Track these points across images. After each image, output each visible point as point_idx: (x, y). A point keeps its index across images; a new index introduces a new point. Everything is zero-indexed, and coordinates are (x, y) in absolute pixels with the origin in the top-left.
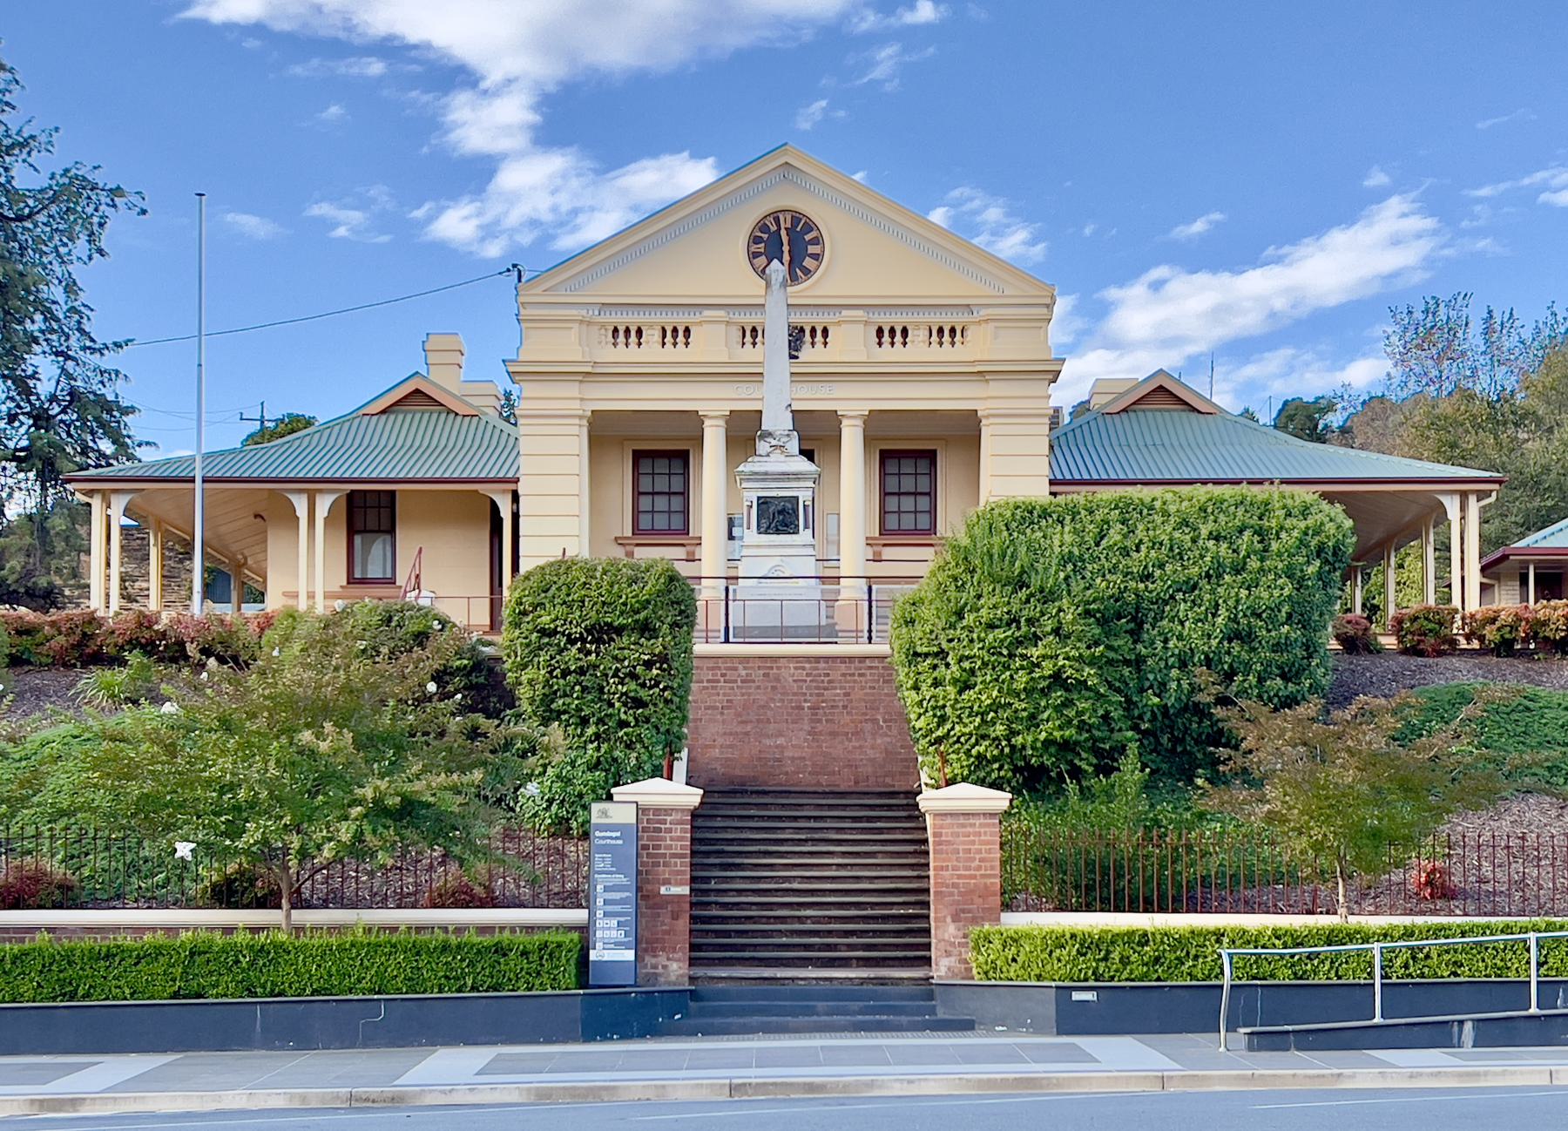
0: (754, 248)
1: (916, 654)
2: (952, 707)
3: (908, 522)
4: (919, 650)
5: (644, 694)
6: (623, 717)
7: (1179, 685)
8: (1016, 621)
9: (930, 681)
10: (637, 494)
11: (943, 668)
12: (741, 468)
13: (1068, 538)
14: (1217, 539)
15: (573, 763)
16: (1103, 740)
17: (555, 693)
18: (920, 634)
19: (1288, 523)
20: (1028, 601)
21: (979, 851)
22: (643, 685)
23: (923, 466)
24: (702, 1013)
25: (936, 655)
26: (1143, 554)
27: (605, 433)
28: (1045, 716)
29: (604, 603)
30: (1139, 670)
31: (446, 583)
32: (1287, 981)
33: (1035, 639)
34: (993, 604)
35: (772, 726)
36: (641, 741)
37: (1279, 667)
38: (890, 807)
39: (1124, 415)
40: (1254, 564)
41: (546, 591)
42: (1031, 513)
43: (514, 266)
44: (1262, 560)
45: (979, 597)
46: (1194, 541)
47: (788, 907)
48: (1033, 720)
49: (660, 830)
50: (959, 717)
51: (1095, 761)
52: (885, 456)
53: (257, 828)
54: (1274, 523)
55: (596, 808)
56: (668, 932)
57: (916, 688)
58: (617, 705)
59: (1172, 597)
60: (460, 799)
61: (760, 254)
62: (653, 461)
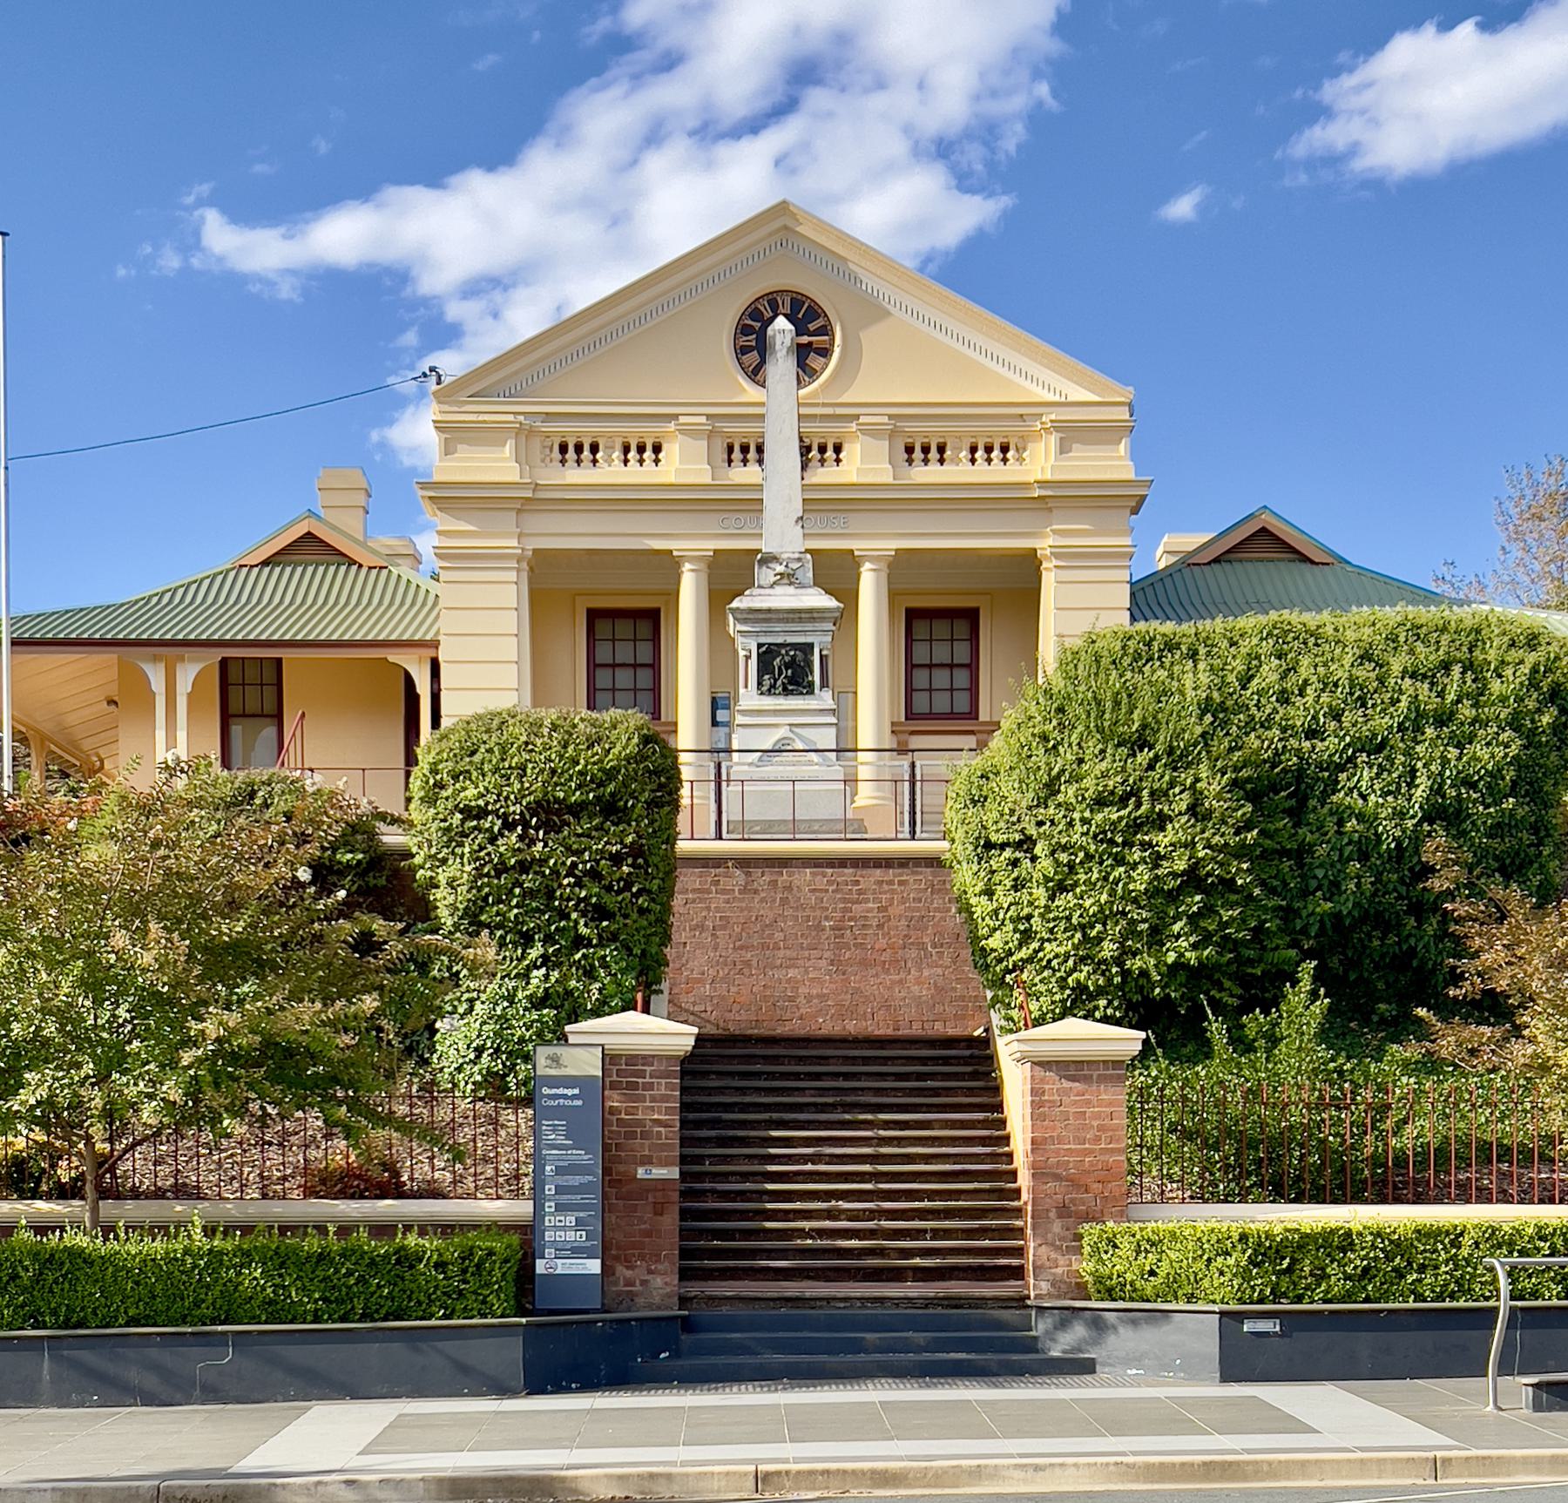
0: (743, 341)
1: (989, 845)
2: (1042, 915)
3: (941, 703)
4: (994, 838)
5: (610, 901)
6: (583, 930)
7: (1358, 885)
8: (1135, 793)
9: (1009, 884)
10: (593, 666)
11: (1027, 863)
12: (735, 604)
13: (1204, 678)
14: (1413, 676)
15: (511, 998)
16: (1251, 962)
17: (485, 899)
18: (995, 815)
19: (1514, 655)
20: (1151, 767)
21: (1097, 1116)
22: (609, 889)
23: (962, 628)
24: (698, 1350)
25: (1018, 845)
26: (1310, 699)
27: (547, 580)
28: (1176, 928)
29: (553, 771)
30: (1301, 865)
31: (337, 766)
32: (1555, 1302)
33: (1161, 822)
34: (1103, 770)
35: (781, 953)
36: (605, 966)
37: (1496, 858)
38: (946, 1061)
39: (1215, 566)
40: (1466, 711)
41: (473, 753)
42: (1149, 644)
43: (432, 369)
44: (1476, 705)
45: (1081, 761)
46: (1381, 681)
47: (798, 1198)
48: (1157, 937)
49: (635, 1086)
50: (1051, 931)
51: (1239, 991)
52: (913, 615)
53: (42, 1082)
54: (1492, 655)
55: (542, 1054)
56: (648, 1233)
57: (989, 893)
58: (574, 915)
59: (1350, 760)
60: (347, 1039)
61: (751, 349)
62: (615, 630)
